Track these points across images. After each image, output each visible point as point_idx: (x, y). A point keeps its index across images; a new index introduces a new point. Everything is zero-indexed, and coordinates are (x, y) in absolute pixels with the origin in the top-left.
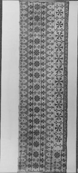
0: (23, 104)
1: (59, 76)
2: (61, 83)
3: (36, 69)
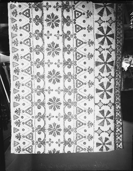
0: (20, 117)
1: (104, 22)
2: (111, 39)
3: (52, 63)
